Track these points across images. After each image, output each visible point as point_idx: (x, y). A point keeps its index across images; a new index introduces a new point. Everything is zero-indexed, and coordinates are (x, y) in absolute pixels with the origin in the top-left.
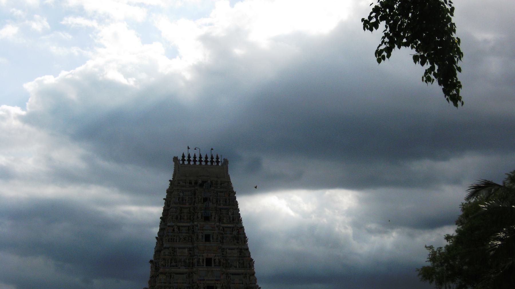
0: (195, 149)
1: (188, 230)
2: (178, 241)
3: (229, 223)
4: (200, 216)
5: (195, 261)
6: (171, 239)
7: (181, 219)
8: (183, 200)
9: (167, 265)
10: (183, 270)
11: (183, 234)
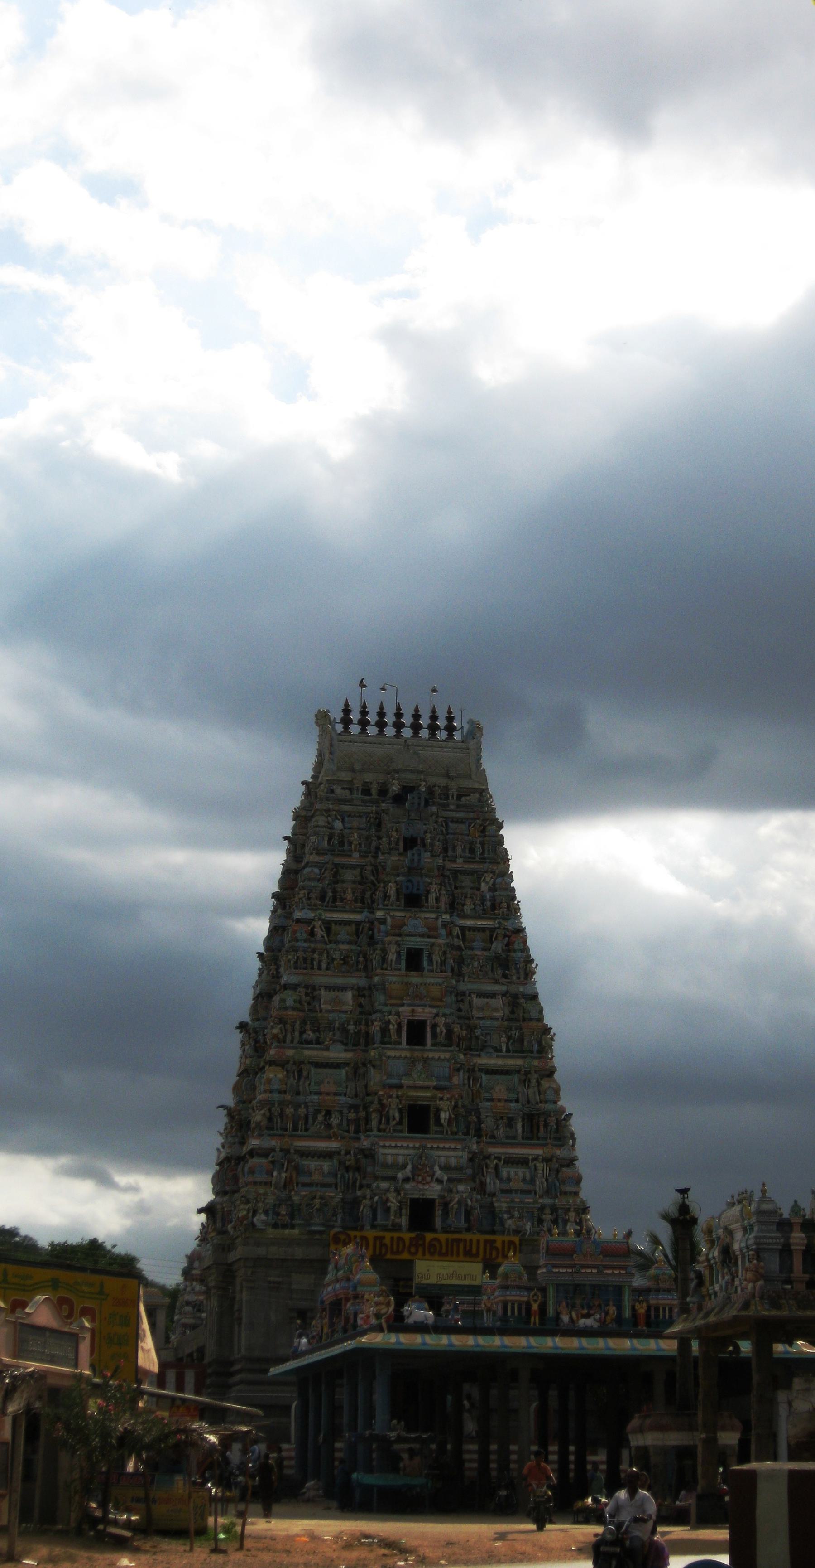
0: (383, 689)
1: (357, 933)
2: (324, 966)
3: (479, 917)
4: (392, 890)
5: (376, 1027)
6: (305, 959)
7: (334, 899)
8: (341, 844)
9: (289, 1037)
10: (338, 1053)
11: (342, 946)
